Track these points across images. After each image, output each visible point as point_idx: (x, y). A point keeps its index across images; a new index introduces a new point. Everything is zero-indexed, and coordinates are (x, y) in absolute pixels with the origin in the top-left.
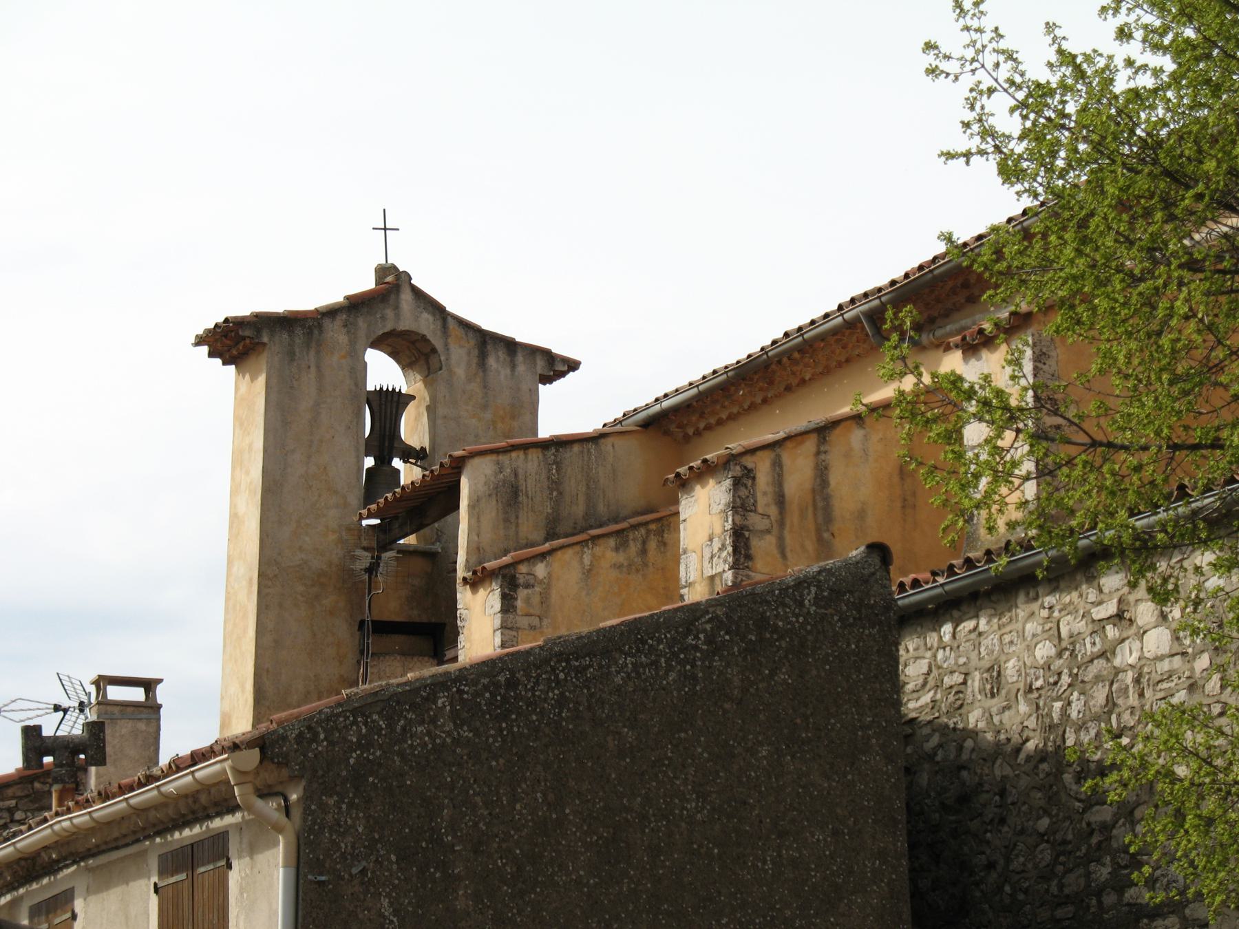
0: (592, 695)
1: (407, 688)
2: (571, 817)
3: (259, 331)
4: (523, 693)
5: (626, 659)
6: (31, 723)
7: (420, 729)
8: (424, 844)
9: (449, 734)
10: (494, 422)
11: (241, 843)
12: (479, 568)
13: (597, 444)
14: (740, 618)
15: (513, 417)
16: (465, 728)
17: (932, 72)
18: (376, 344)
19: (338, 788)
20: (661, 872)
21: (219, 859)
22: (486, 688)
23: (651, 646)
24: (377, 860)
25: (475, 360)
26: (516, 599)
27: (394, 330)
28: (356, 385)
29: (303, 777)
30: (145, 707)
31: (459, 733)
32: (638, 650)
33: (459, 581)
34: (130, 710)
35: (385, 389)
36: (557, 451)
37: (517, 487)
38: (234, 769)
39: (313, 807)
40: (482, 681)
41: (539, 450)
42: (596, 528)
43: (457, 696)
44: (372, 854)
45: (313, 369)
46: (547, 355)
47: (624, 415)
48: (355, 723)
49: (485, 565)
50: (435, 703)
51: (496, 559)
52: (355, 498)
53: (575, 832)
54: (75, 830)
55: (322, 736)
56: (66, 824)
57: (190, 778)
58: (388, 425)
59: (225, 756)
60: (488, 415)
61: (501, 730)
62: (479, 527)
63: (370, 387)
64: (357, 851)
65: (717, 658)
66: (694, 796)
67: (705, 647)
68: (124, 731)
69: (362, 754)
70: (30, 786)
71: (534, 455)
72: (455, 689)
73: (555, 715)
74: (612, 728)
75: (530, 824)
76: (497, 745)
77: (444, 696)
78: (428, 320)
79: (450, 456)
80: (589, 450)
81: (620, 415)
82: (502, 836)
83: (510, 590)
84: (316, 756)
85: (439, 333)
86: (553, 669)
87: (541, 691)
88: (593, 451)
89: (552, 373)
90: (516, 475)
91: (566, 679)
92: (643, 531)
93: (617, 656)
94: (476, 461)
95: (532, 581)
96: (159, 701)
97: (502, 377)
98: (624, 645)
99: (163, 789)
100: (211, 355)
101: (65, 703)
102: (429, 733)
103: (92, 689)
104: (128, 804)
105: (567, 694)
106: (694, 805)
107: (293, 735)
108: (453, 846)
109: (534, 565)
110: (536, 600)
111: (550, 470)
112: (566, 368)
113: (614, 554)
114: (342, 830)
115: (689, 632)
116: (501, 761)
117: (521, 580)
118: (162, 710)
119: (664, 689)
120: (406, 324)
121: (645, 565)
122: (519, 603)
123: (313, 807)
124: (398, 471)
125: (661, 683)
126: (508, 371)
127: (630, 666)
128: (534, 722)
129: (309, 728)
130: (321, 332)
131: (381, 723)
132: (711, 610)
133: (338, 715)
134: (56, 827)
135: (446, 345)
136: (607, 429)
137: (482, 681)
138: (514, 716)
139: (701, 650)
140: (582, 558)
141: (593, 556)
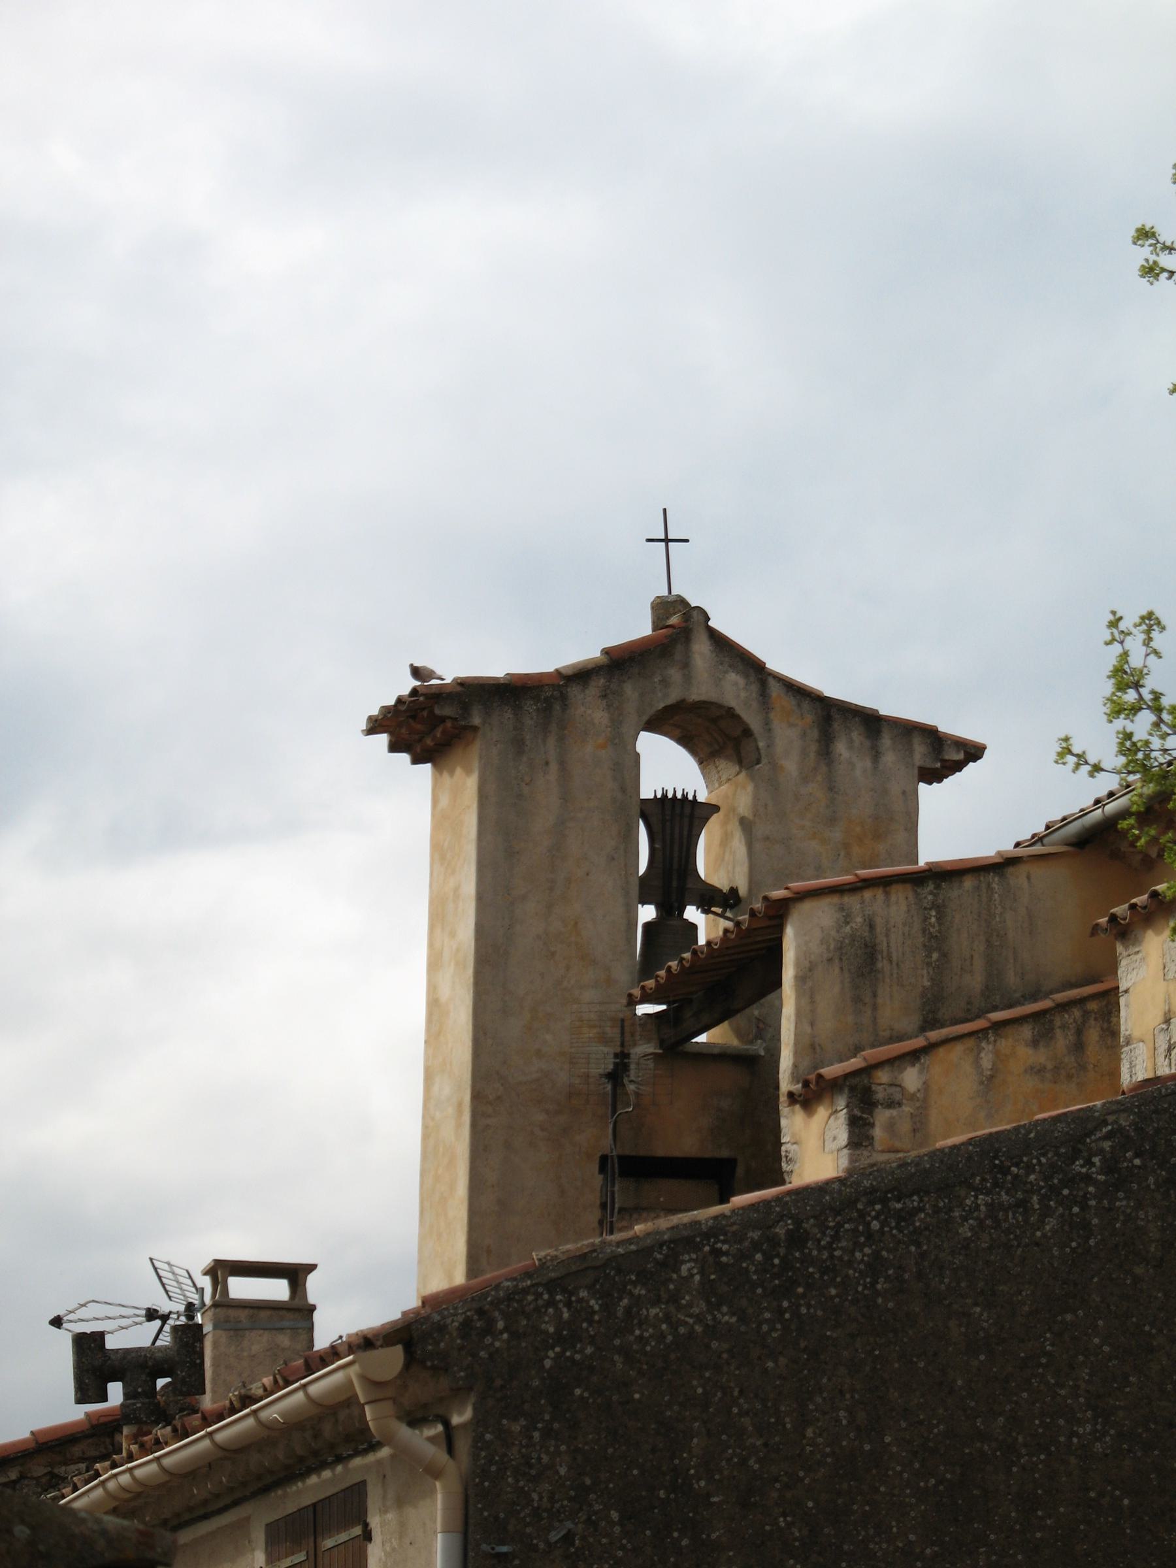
0: (923, 1255)
1: (633, 1247)
2: (894, 1449)
3: (466, 708)
4: (815, 1253)
5: (976, 1197)
6: (88, 1328)
7: (654, 1311)
8: (662, 1494)
9: (699, 1319)
10: (846, 846)
11: (384, 1497)
12: (812, 1077)
13: (1002, 876)
14: (1158, 1131)
15: (878, 836)
16: (725, 1309)
17: (1151, 271)
18: (655, 725)
19: (526, 1406)
20: (1038, 1535)
21: (353, 1524)
22: (756, 1246)
23: (1016, 1177)
24: (589, 1519)
25: (813, 748)
26: (872, 1125)
27: (683, 701)
28: (623, 790)
29: (470, 1389)
30: (289, 1310)
31: (714, 1318)
32: (996, 1184)
33: (783, 1099)
34: (264, 1314)
35: (670, 795)
36: (938, 887)
37: (874, 946)
38: (364, 1378)
39: (488, 1437)
40: (750, 1234)
41: (908, 886)
42: (1002, 1009)
43: (711, 1259)
44: (581, 1509)
45: (554, 767)
46: (931, 735)
47: (1048, 827)
48: (552, 1303)
49: (822, 1071)
50: (677, 1270)
51: (842, 1061)
52: (624, 975)
53: (901, 1473)
54: (139, 1490)
55: (501, 1325)
56: (125, 1479)
57: (300, 1396)
58: (676, 854)
59: (351, 1357)
60: (837, 834)
61: (781, 1312)
62: (813, 1011)
63: (646, 793)
64: (557, 1505)
65: (1121, 1195)
66: (1089, 1414)
67: (1101, 1178)
68: (256, 1348)
69: (564, 1351)
70: (108, 1440)
71: (901, 897)
72: (707, 1248)
73: (865, 1287)
74: (955, 1306)
75: (829, 1460)
76: (775, 1335)
77: (690, 1260)
78: (736, 684)
79: (766, 898)
80: (989, 885)
81: (1040, 828)
82: (785, 1479)
83: (863, 1111)
84: (491, 1355)
85: (755, 705)
86: (862, 1215)
87: (841, 1248)
88: (995, 886)
89: (938, 765)
90: (872, 927)
91: (881, 1231)
92: (1077, 1013)
93: (963, 1193)
94: (807, 906)
95: (898, 1097)
96: (311, 1300)
97: (858, 772)
98: (973, 1175)
99: (263, 1415)
100: (394, 748)
101: (165, 1306)
102: (667, 1318)
103: (206, 1282)
104: (213, 1441)
105: (884, 1253)
106: (1089, 1428)
107: (456, 1324)
108: (709, 1495)
109: (902, 1070)
110: (905, 1127)
111: (926, 919)
112: (961, 756)
113: (1030, 1051)
114: (533, 1472)
115: (1075, 1155)
116: (783, 1361)
117: (880, 1094)
118: (316, 1315)
119: (1037, 1244)
120: (702, 690)
121: (1082, 1067)
122: (878, 1132)
123: (488, 1437)
124: (694, 927)
125: (1033, 1234)
126: (868, 764)
127: (983, 1208)
128: (832, 1298)
129: (481, 1312)
130: (565, 708)
131: (592, 1302)
132: (1111, 1118)
133: (525, 1291)
134: (111, 1485)
135: (767, 723)
136: (1020, 852)
137: (750, 1234)
138: (800, 1290)
139: (1095, 1183)
140: (977, 1059)
141: (997, 1053)
